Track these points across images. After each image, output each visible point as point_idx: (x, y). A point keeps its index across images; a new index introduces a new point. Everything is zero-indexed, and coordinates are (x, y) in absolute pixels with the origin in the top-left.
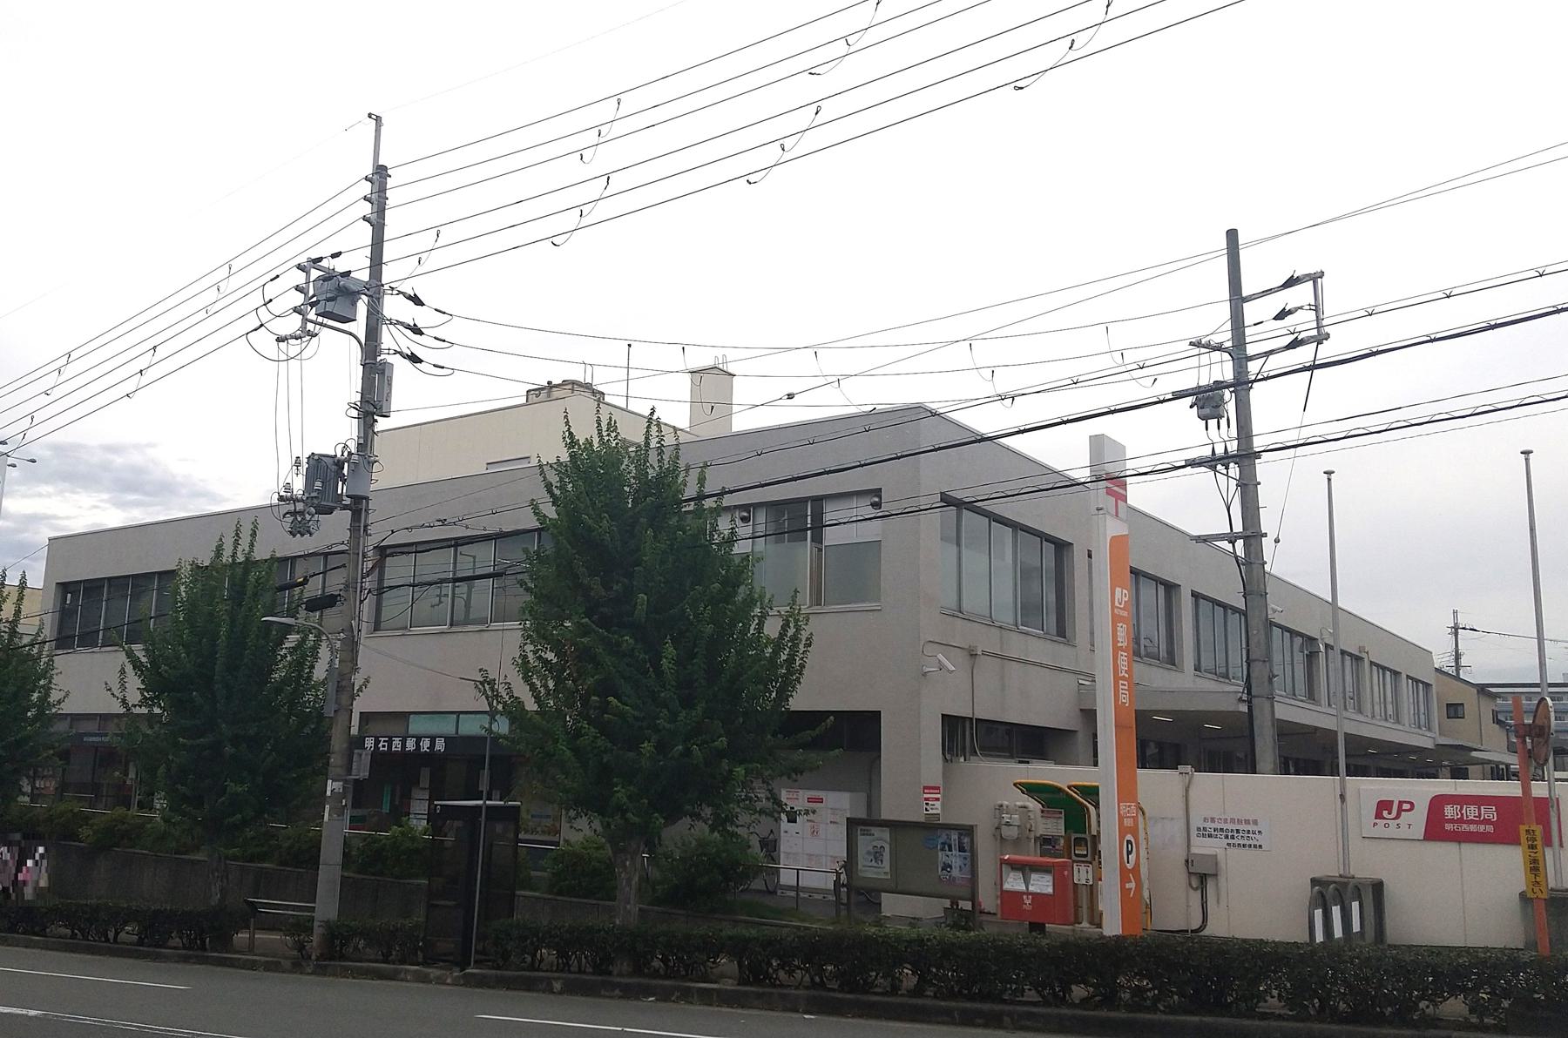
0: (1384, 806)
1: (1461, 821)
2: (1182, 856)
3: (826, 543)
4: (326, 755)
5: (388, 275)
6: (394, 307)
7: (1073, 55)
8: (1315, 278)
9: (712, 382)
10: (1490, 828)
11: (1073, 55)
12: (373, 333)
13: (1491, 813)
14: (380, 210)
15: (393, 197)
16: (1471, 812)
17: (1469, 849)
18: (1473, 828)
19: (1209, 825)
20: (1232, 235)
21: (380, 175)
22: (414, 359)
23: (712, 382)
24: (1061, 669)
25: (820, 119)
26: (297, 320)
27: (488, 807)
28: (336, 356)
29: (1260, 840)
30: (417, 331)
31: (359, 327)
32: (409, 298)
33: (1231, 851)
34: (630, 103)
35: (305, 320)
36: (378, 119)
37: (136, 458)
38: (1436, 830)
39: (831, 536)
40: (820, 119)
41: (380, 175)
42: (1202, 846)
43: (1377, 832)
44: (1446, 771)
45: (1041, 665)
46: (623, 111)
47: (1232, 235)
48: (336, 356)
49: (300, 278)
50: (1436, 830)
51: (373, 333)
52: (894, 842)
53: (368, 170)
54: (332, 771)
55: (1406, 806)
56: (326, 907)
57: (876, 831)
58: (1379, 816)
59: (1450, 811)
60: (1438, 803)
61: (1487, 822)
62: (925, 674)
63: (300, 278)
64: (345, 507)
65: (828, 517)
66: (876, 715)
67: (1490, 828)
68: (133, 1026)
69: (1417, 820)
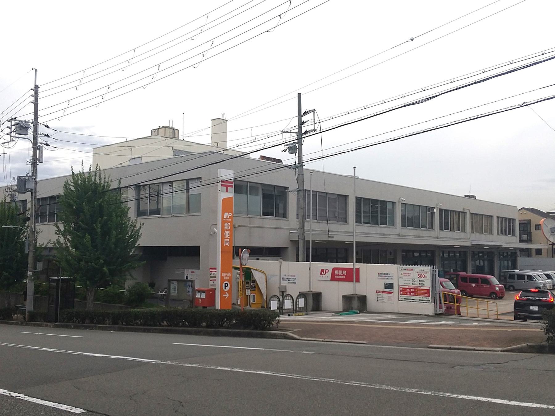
0: (322, 271)
1: (338, 275)
2: (278, 285)
3: (190, 194)
4: (27, 264)
5: (40, 120)
6: (42, 129)
7: (154, 80)
8: (314, 110)
9: (219, 124)
10: (344, 277)
11: (154, 80)
12: (35, 138)
13: (345, 273)
14: (36, 99)
15: (40, 95)
16: (341, 272)
17: (341, 283)
18: (341, 277)
19: (285, 277)
20: (299, 95)
21: (37, 87)
22: (48, 145)
23: (219, 124)
24: (281, 228)
25: (110, 90)
26: (8, 137)
27: (62, 279)
28: (23, 146)
29: (296, 281)
30: (47, 136)
31: (31, 135)
32: (45, 126)
33: (290, 285)
34: (88, 73)
35: (11, 137)
36: (36, 70)
37: (87, 132)
38: (333, 278)
39: (191, 192)
40: (110, 90)
41: (37, 87)
42: (284, 283)
43: (321, 278)
44: (399, 259)
45: (270, 228)
46: (86, 75)
47: (299, 95)
48: (23, 146)
49: (9, 124)
50: (333, 278)
51: (35, 138)
52: (178, 283)
53: (33, 87)
54: (29, 269)
55: (327, 271)
56: (29, 306)
57: (174, 282)
58: (321, 274)
59: (336, 272)
60: (334, 269)
61: (344, 275)
62: (211, 235)
63: (9, 124)
64: (28, 191)
65: (191, 186)
66: (198, 247)
67: (344, 277)
68: (485, 399)
69: (329, 274)
